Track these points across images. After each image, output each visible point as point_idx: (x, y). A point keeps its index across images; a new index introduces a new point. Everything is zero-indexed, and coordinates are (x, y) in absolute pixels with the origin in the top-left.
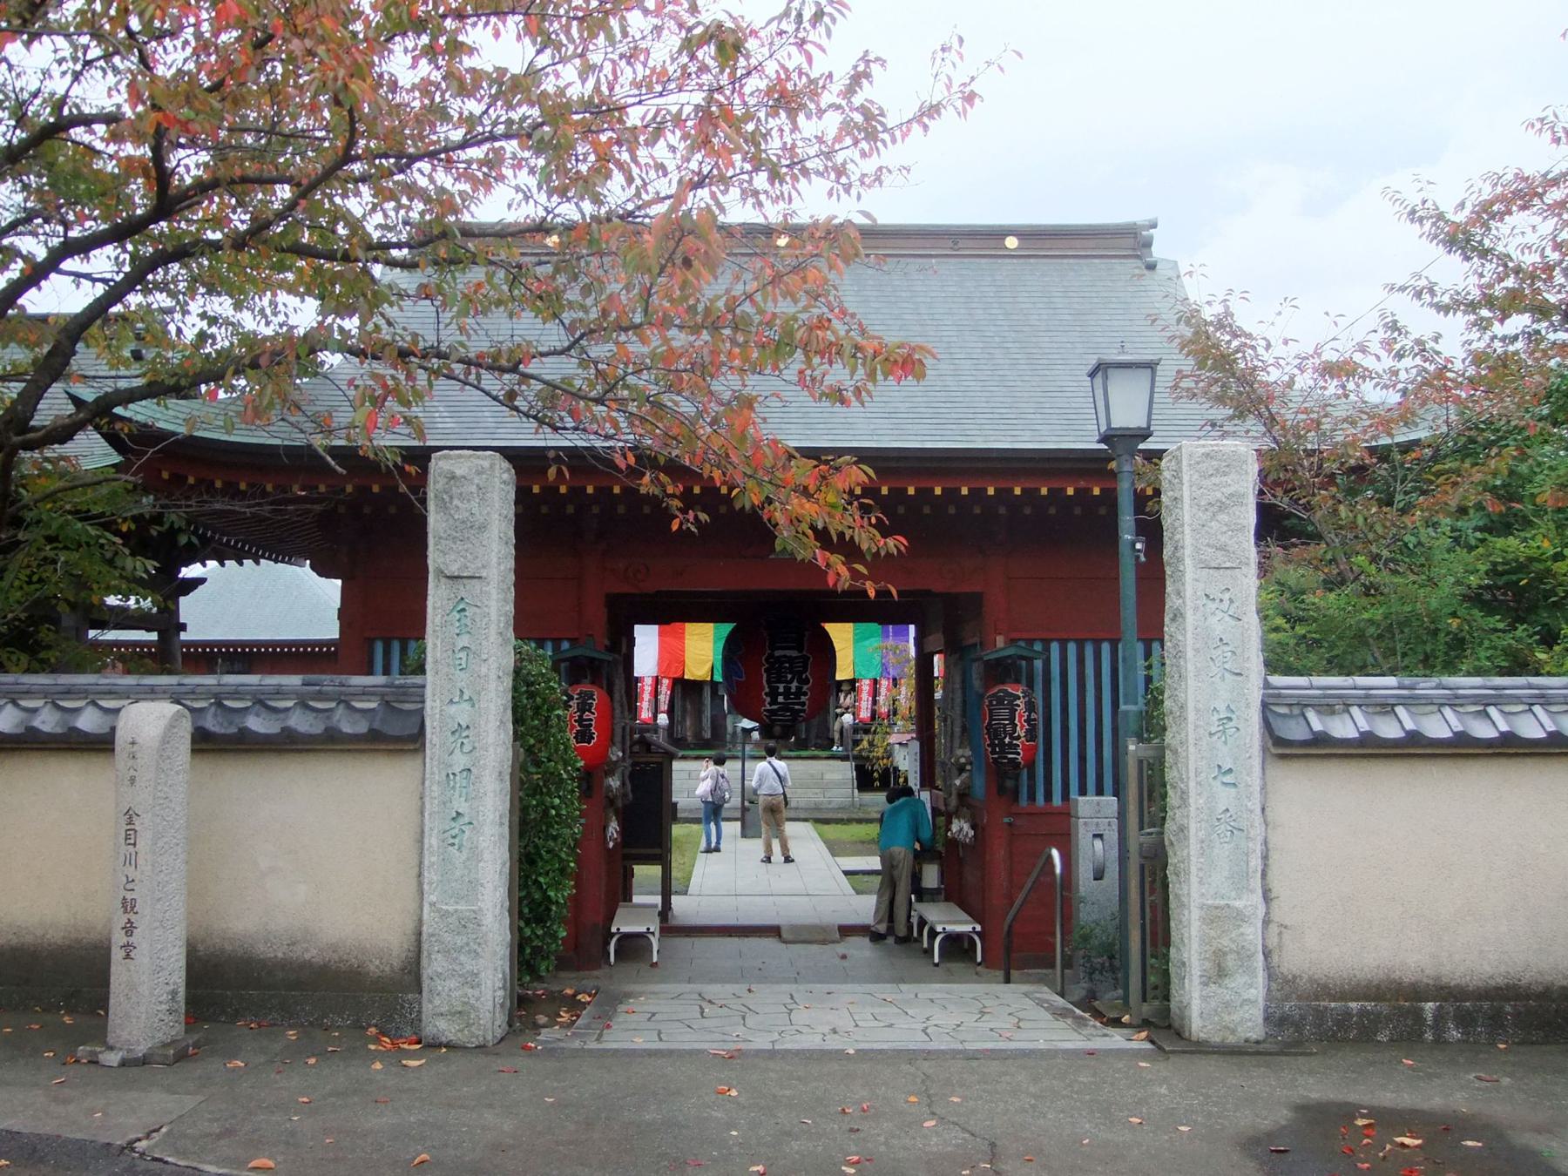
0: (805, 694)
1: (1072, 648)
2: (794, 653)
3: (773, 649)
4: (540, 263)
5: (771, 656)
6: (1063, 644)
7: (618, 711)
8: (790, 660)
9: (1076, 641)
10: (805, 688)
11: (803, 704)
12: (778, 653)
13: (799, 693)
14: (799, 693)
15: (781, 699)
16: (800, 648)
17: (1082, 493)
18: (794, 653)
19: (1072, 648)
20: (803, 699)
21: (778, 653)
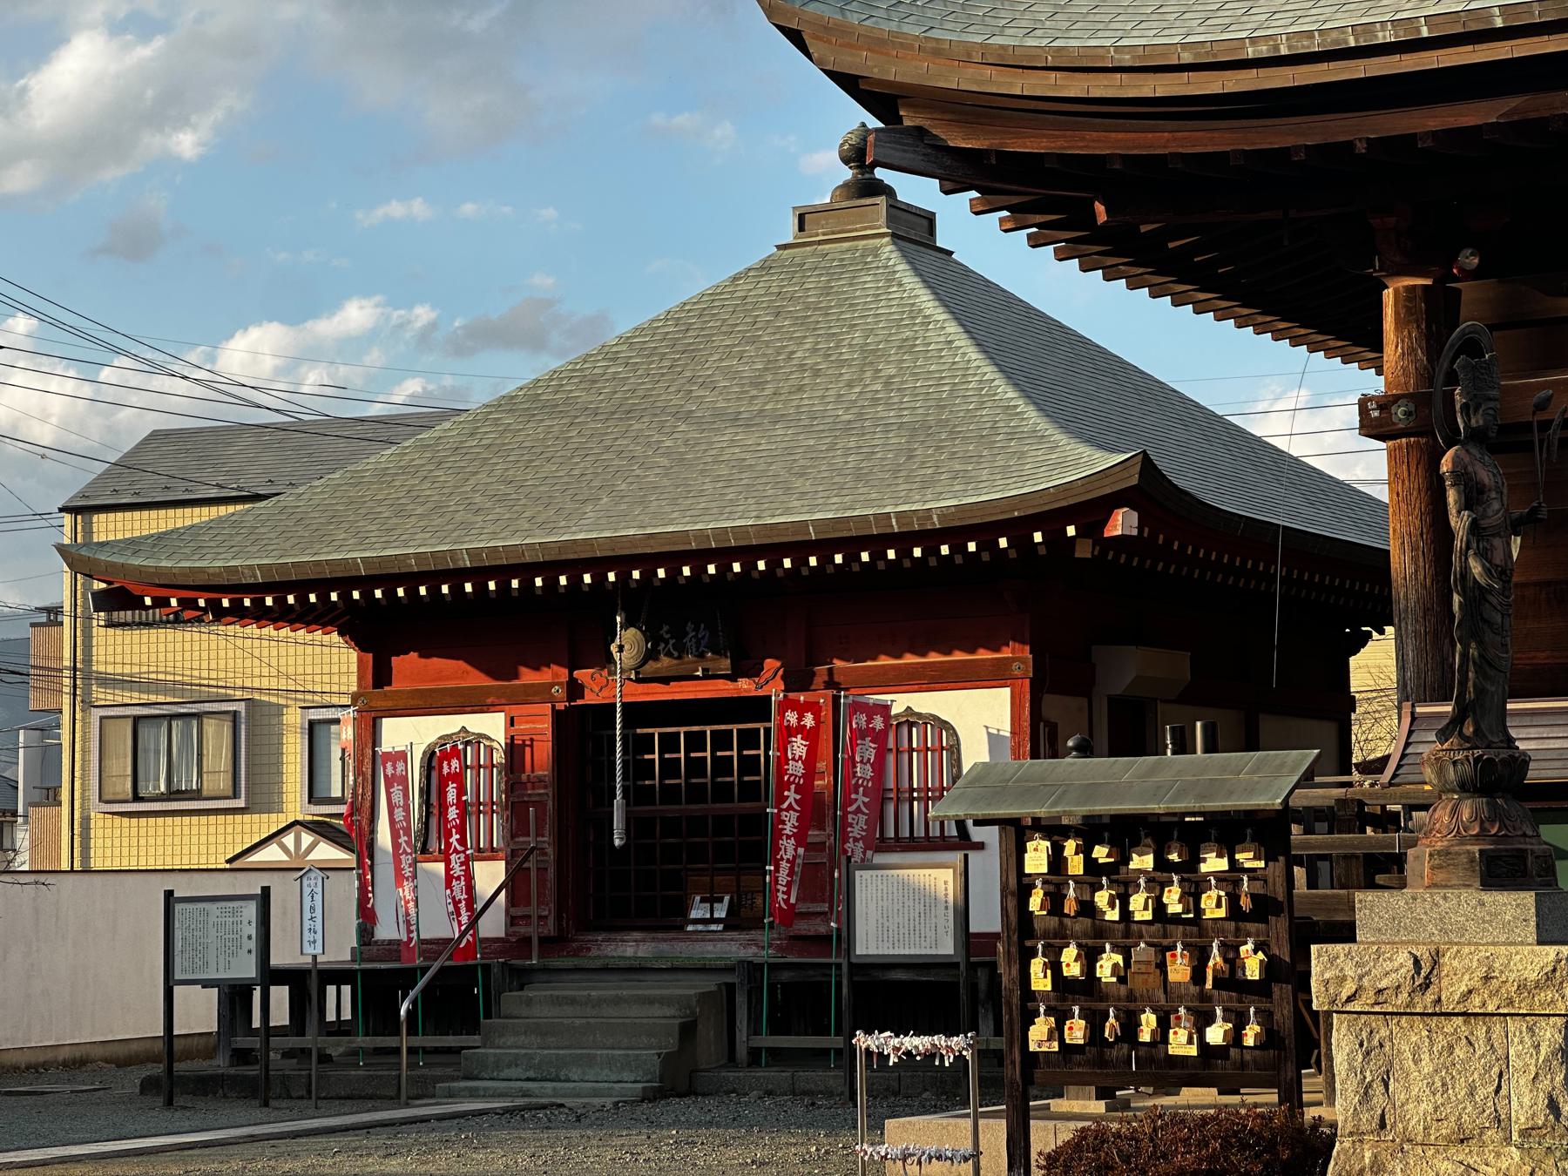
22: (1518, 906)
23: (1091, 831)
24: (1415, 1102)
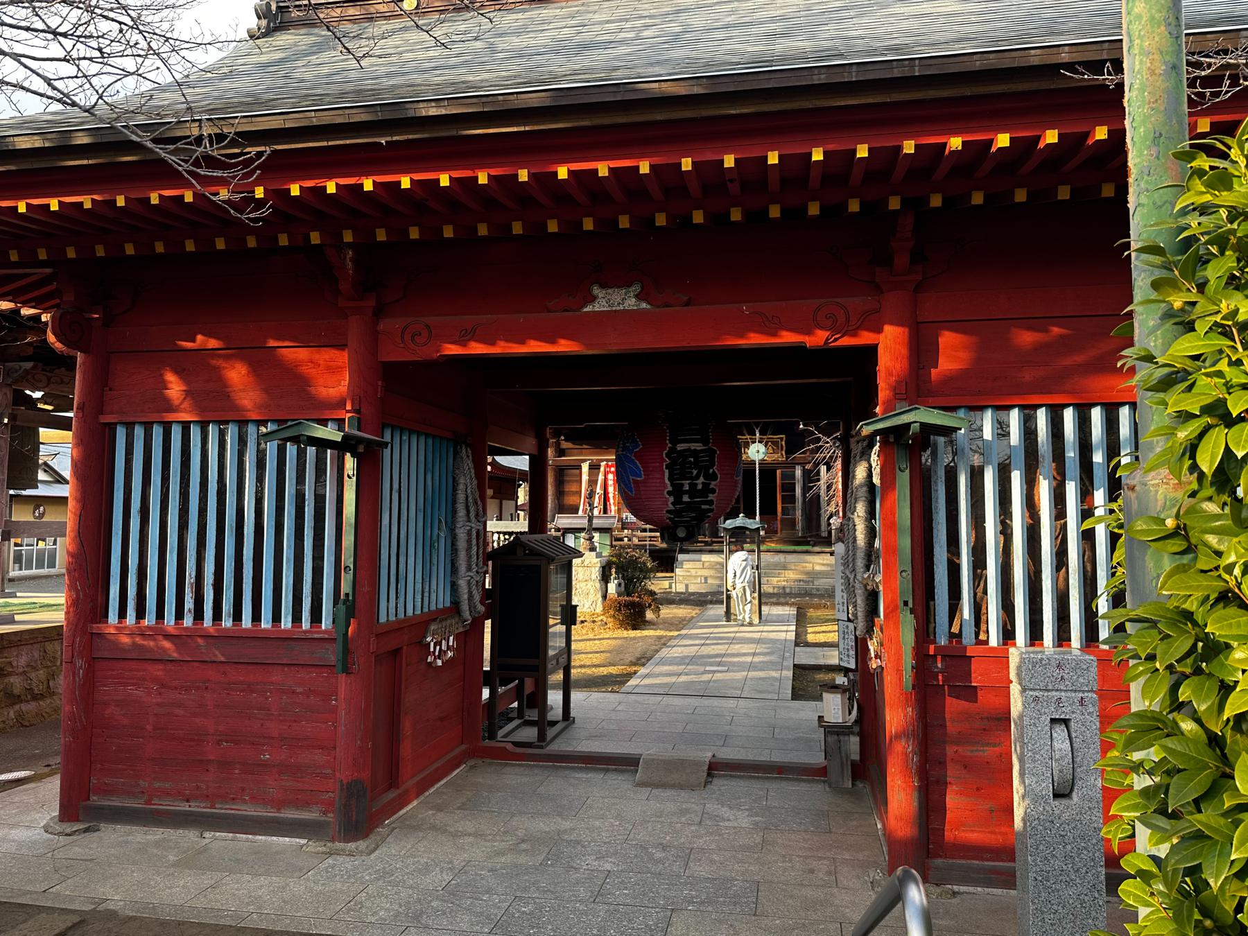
0: (713, 491)
1: (139, 432)
2: (698, 446)
3: (675, 442)
4: (647, 27)
5: (673, 450)
6: (148, 427)
7: (461, 513)
8: (695, 453)
9: (1022, 407)
10: (713, 484)
11: (711, 503)
12: (680, 447)
13: (707, 489)
14: (707, 489)
15: (686, 498)
16: (705, 443)
17: (1073, 143)
18: (698, 446)
19: (139, 432)
20: (711, 497)
21: (680, 447)
22: (594, 554)
23: (505, 533)
24: (580, 577)
